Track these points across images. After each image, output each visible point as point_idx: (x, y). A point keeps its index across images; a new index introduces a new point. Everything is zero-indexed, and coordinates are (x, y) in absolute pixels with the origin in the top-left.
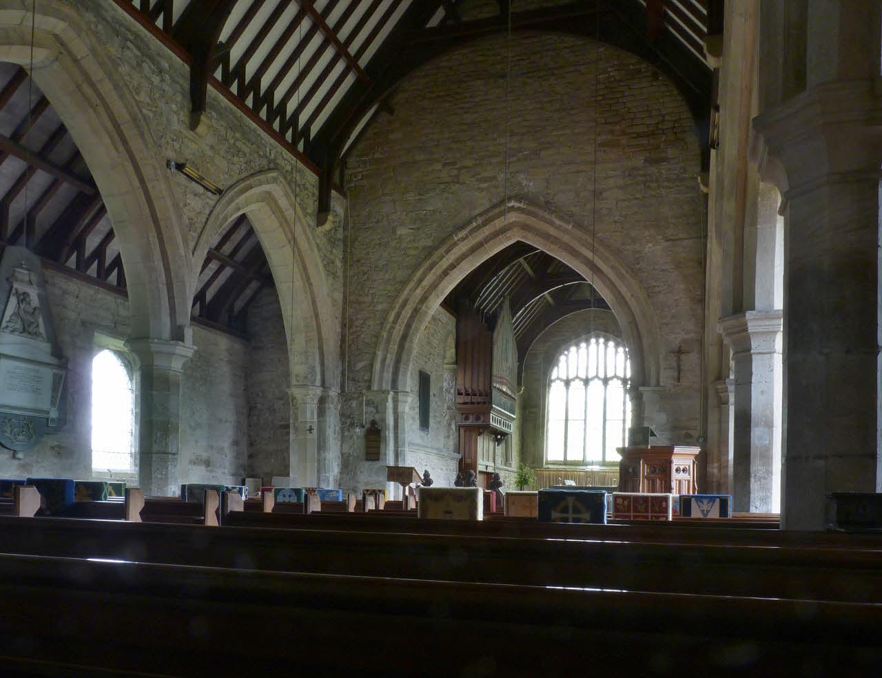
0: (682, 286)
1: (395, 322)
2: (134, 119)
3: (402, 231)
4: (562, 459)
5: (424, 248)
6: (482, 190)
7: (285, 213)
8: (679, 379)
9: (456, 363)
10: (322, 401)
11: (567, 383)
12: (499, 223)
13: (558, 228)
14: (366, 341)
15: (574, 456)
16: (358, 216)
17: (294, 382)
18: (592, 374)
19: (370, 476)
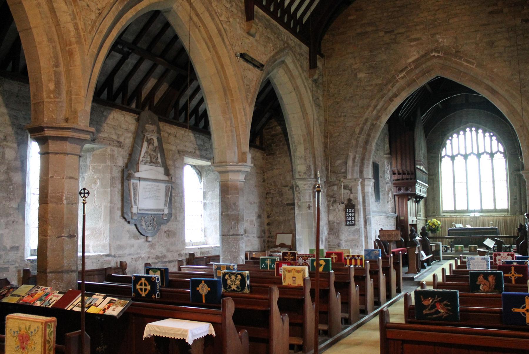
1: (360, 133)
2: (219, 31)
3: (361, 75)
4: (453, 209)
6: (412, 46)
7: (293, 72)
9: (390, 153)
11: (453, 158)
15: (461, 206)
17: (297, 176)
18: (469, 151)
19: (348, 236)
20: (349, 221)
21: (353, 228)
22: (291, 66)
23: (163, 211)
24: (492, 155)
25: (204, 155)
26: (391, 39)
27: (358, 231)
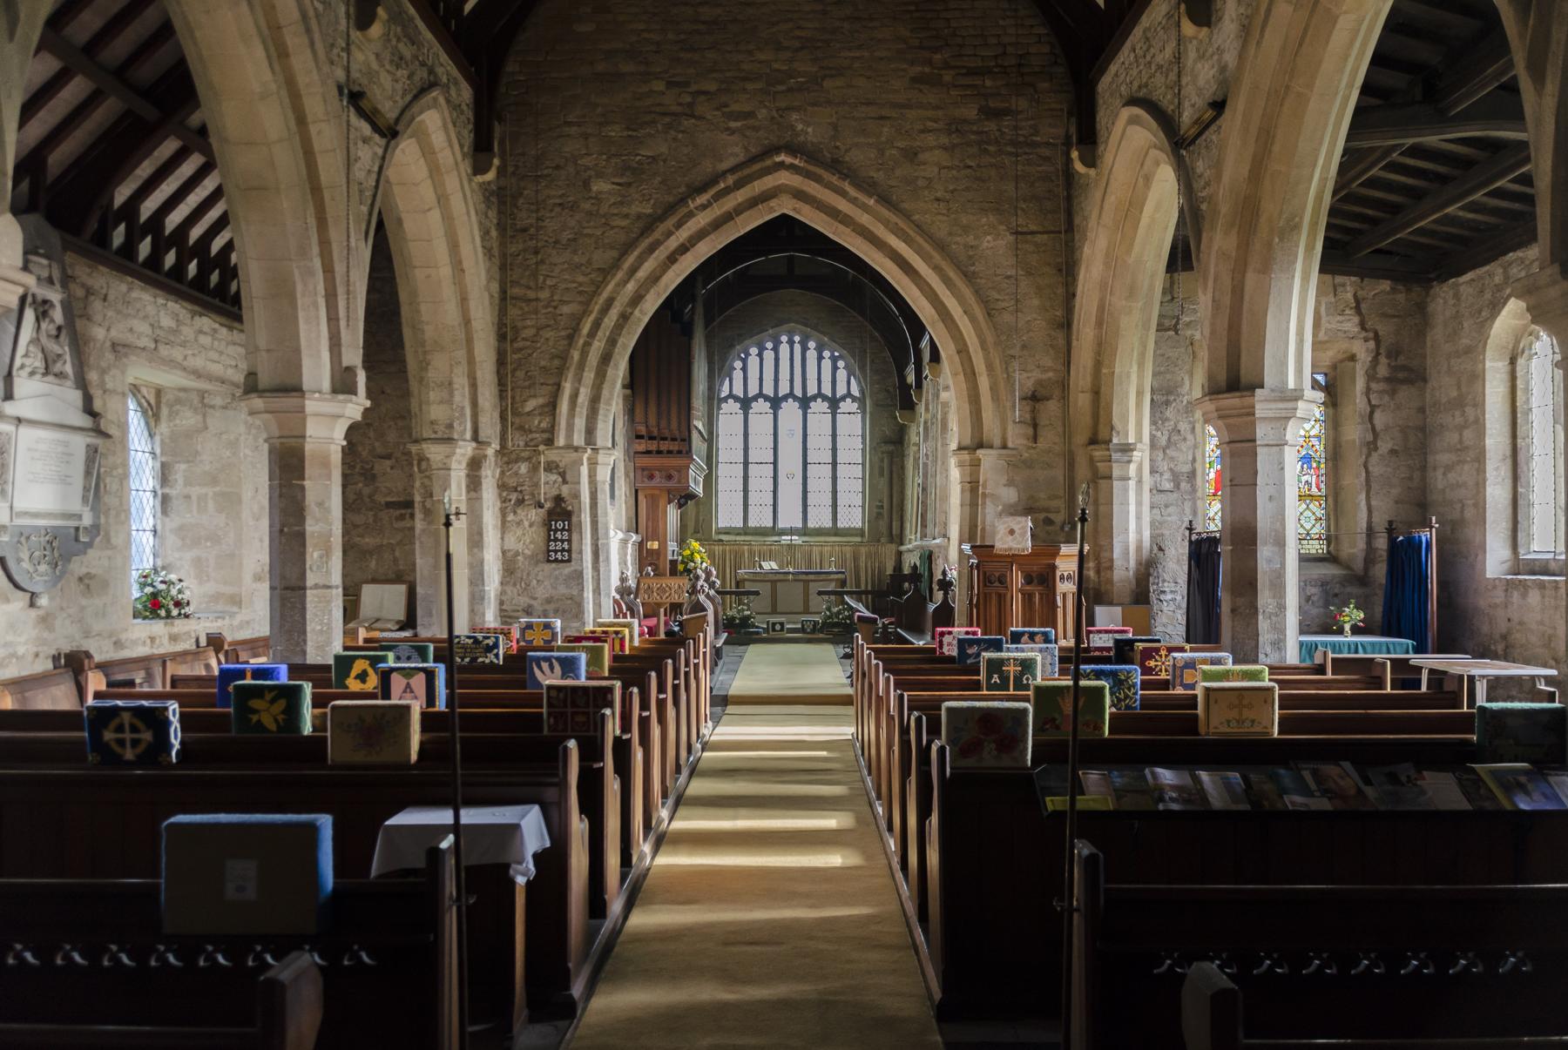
0: (1036, 302)
3: (599, 186)
5: (639, 216)
6: (732, 132)
8: (1035, 439)
10: (475, 464)
11: (746, 403)
12: (758, 186)
13: (854, 201)
14: (543, 363)
15: (760, 518)
16: (523, 154)
20: (556, 552)
21: (567, 570)
23: (80, 517)
24: (834, 403)
25: (180, 358)
26: (680, 104)
27: (579, 575)
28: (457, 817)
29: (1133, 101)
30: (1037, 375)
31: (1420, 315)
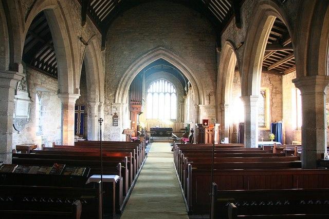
6: (151, 43)
10: (99, 106)
11: (153, 94)
18: (166, 92)
22: (95, 44)
24: (171, 94)
28: (102, 177)
29: (227, 40)
30: (210, 90)
31: (281, 80)
